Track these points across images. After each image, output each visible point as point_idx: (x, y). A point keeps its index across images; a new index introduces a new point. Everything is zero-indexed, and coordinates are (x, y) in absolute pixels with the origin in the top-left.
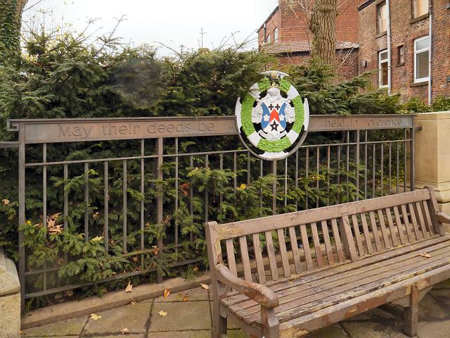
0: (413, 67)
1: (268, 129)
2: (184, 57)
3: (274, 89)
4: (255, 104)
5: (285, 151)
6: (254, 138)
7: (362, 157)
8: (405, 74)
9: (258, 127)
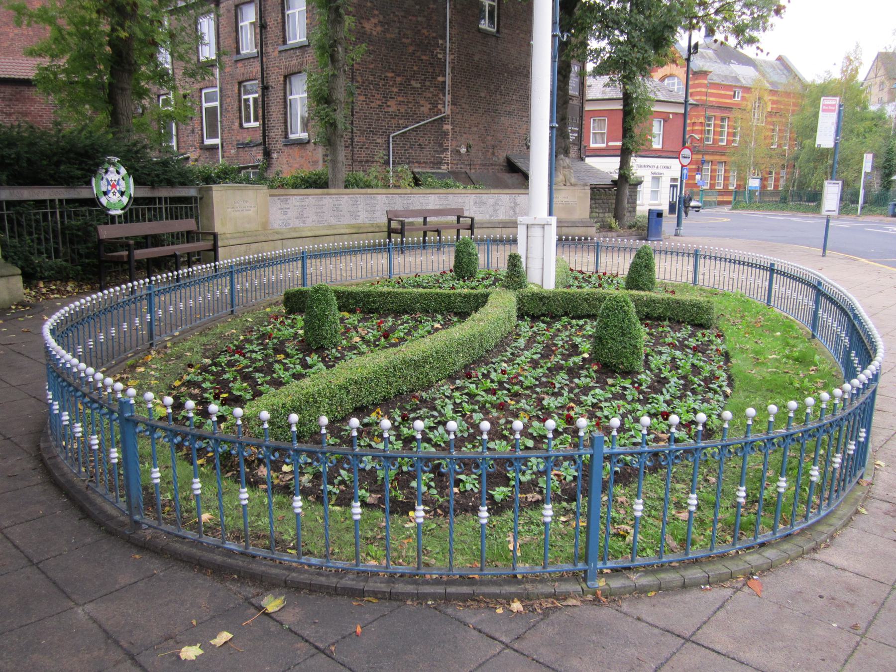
0: (202, 123)
1: (111, 195)
2: (106, 165)
3: (112, 169)
4: (102, 179)
5: (122, 209)
6: (104, 200)
7: (247, 107)
8: (193, 131)
9: (105, 193)
